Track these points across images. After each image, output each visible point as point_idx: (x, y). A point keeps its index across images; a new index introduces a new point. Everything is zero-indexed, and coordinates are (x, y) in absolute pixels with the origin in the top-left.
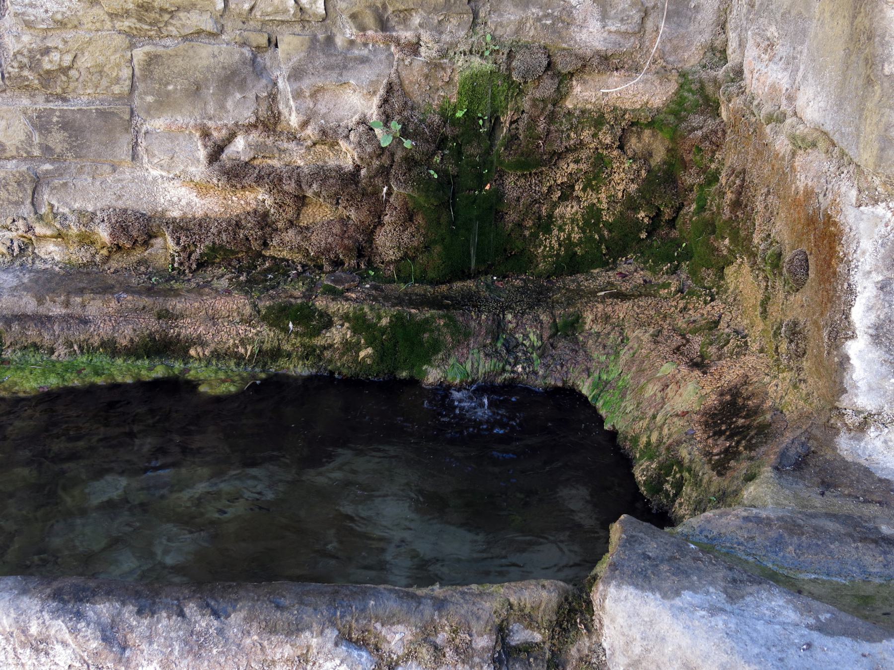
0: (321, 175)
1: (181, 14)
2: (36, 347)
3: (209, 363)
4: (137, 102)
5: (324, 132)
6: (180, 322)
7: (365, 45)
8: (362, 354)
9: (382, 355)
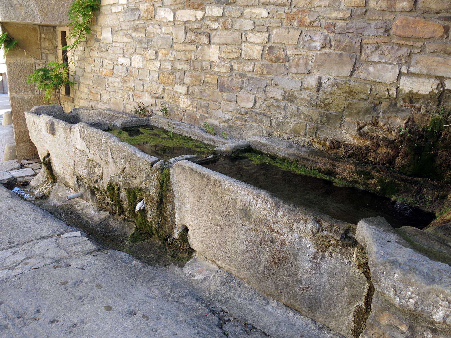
0: (384, 139)
1: (359, 94)
2: (305, 166)
3: (340, 180)
4: (344, 114)
5: (388, 128)
6: (337, 168)
7: (405, 107)
8: (377, 187)
9: (382, 189)
